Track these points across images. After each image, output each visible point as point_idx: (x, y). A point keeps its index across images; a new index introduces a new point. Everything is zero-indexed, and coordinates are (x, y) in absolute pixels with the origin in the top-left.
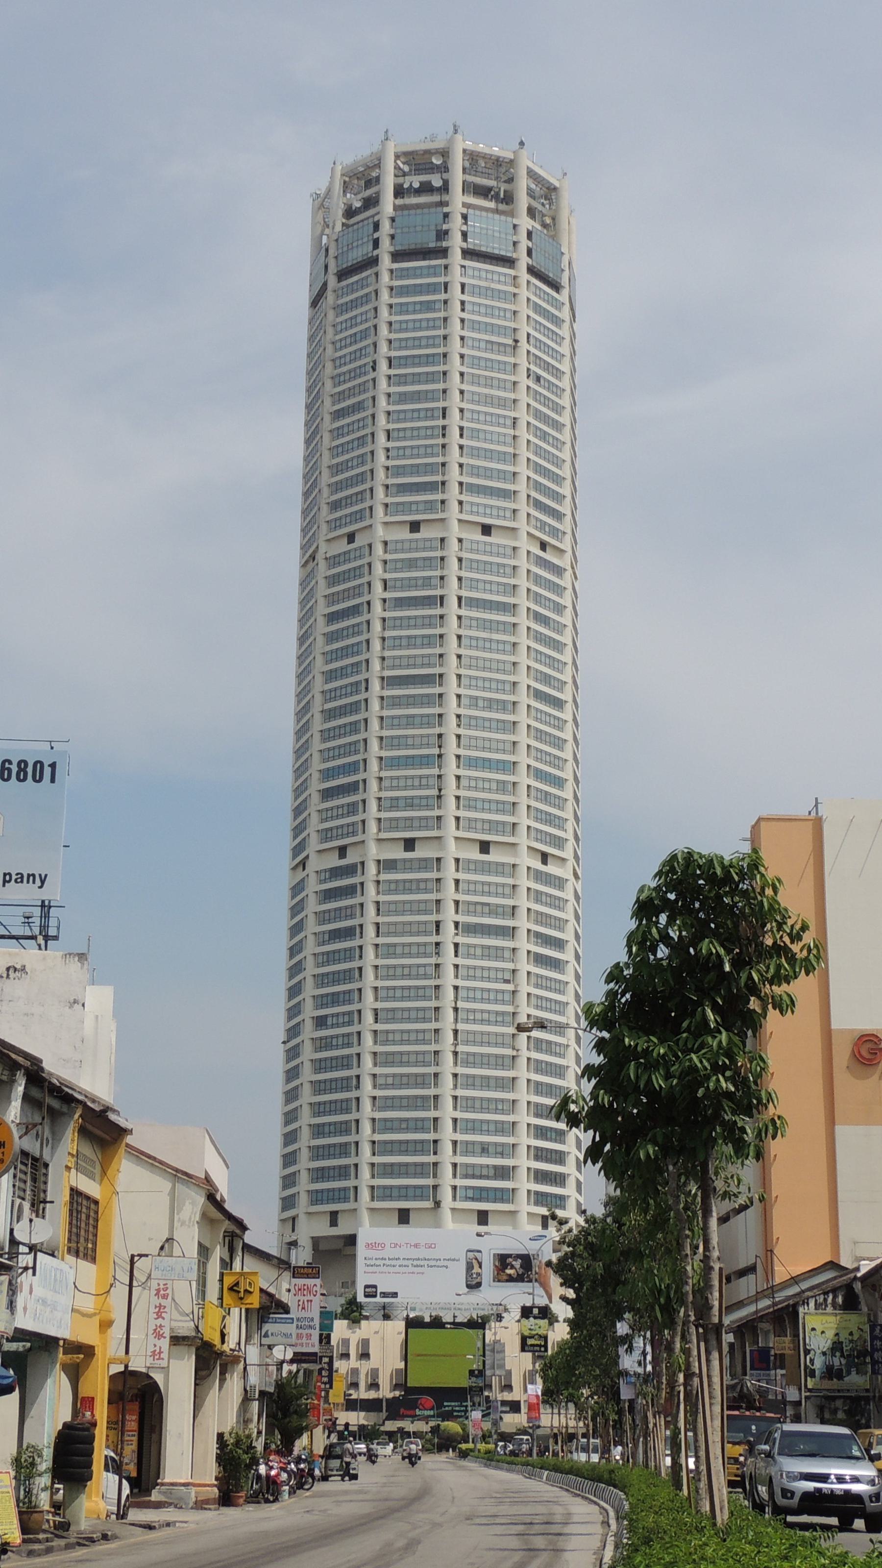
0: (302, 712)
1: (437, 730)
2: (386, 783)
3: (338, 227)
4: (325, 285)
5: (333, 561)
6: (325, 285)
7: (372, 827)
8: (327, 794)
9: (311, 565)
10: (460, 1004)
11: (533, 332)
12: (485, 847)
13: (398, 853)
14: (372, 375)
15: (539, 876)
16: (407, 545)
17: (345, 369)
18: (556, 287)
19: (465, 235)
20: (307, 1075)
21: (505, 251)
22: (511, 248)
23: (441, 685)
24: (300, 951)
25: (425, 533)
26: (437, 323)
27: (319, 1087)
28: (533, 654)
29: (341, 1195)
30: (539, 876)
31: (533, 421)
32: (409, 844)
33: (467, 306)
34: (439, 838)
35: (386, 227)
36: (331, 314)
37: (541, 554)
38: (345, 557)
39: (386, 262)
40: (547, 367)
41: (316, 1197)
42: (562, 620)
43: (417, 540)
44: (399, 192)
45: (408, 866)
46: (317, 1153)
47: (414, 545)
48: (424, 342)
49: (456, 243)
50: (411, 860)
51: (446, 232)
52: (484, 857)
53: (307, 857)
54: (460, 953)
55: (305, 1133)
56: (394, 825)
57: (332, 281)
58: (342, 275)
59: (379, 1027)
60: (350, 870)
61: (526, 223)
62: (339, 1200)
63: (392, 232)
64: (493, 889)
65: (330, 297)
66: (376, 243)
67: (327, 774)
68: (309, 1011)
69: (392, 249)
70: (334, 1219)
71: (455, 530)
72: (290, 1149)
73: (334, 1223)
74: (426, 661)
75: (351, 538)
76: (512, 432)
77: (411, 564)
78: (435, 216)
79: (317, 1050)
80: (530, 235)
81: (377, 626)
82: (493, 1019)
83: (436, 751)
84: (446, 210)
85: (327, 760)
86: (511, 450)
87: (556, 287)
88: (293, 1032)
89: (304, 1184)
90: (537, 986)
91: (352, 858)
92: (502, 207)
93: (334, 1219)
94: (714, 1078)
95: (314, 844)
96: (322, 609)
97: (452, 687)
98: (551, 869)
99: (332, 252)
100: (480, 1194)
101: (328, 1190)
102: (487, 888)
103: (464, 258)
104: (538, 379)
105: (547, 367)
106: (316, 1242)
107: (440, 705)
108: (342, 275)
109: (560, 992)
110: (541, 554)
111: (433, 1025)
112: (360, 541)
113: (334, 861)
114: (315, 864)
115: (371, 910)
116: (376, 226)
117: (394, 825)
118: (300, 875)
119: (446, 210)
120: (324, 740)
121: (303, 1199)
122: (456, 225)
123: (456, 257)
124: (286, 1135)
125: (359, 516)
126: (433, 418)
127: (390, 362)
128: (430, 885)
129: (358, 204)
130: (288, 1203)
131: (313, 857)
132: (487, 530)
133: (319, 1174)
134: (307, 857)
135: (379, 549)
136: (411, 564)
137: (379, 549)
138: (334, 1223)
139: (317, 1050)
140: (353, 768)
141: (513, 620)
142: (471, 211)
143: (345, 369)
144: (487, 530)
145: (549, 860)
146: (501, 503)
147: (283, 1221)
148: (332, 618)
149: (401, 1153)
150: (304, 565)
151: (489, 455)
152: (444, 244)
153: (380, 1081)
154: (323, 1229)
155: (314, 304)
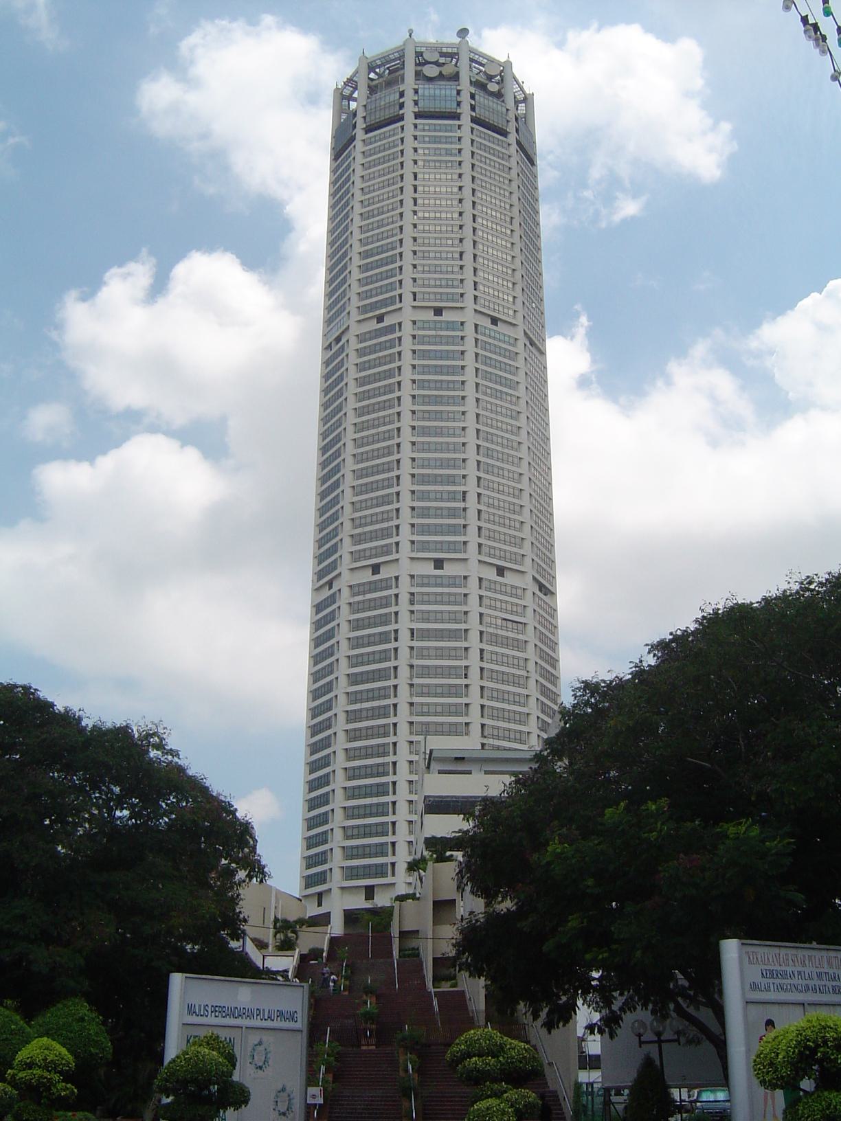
12: (501, 571)
23: (466, 639)
26: (455, 283)
33: (485, 656)
41: (350, 873)
43: (441, 577)
47: (439, 598)
48: (445, 385)
52: (499, 579)
53: (340, 574)
54: (484, 639)
56: (425, 547)
58: (368, 130)
59: (415, 644)
62: (376, 875)
69: (410, 859)
70: (370, 892)
74: (452, 599)
79: (349, 759)
85: (356, 628)
101: (365, 786)
106: (351, 917)
116: (402, 95)
117: (425, 547)
120: (348, 721)
125: (386, 550)
126: (455, 500)
127: (412, 634)
128: (458, 463)
132: (495, 321)
139: (349, 759)
144: (495, 321)
149: (436, 373)
154: (358, 902)
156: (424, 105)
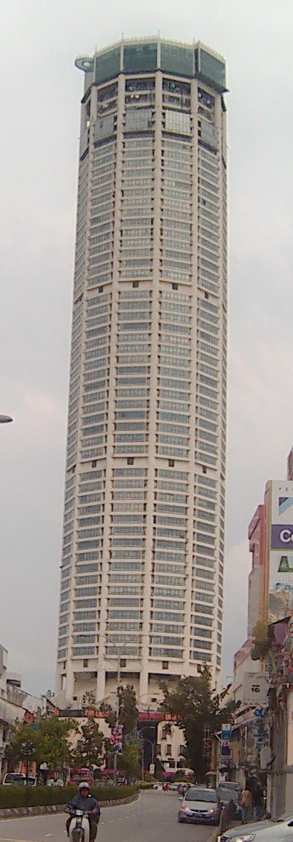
0: (64, 596)
1: (146, 398)
2: (121, 338)
3: (95, 118)
4: (87, 150)
5: (91, 302)
6: (87, 150)
9: (79, 303)
10: (155, 573)
11: (201, 177)
13: (124, 465)
14: (107, 377)
15: (201, 479)
16: (131, 295)
17: (92, 360)
18: (215, 151)
19: (164, 123)
20: (73, 584)
21: (186, 131)
22: (189, 130)
24: (71, 517)
25: (142, 287)
28: (199, 410)
29: (90, 651)
30: (201, 479)
31: (201, 167)
32: (130, 460)
34: (147, 457)
35: (121, 119)
36: (91, 166)
37: (205, 299)
39: (120, 138)
42: (217, 358)
44: (128, 99)
45: (130, 472)
46: (79, 604)
49: (158, 128)
50: (131, 469)
51: (154, 122)
58: (96, 145)
60: (97, 474)
61: (196, 117)
63: (124, 112)
64: (172, 605)
65: (91, 156)
66: (115, 127)
68: (75, 539)
71: (156, 286)
72: (63, 625)
73: (85, 666)
75: (101, 289)
76: (189, 153)
78: (147, 114)
80: (199, 123)
81: (114, 338)
82: (177, 441)
83: (146, 409)
84: (153, 110)
86: (189, 252)
87: (215, 151)
89: (70, 643)
90: (200, 493)
91: (100, 466)
92: (185, 108)
95: (79, 459)
97: (154, 373)
98: (210, 300)
99: (92, 132)
100: (168, 652)
102: (172, 486)
103: (163, 136)
104: (204, 202)
107: (149, 372)
108: (96, 145)
109: (215, 354)
110: (205, 299)
111: (145, 444)
112: (106, 291)
113: (89, 468)
114: (80, 469)
116: (116, 118)
117: (122, 449)
118: (72, 475)
119: (153, 110)
120: (84, 401)
121: (70, 652)
122: (158, 118)
123: (159, 136)
124: (62, 606)
129: (106, 106)
130: (61, 653)
131: (78, 466)
132: (175, 286)
133: (79, 638)
134: (75, 466)
135: (116, 296)
137: (116, 296)
138: (85, 666)
140: (100, 417)
141: (187, 425)
142: (167, 111)
143: (92, 360)
144: (175, 286)
145: (208, 471)
146: (184, 271)
147: (59, 663)
148: (87, 388)
150: (76, 303)
152: (153, 129)
153: (112, 590)
155: (82, 159)
156: (132, 126)
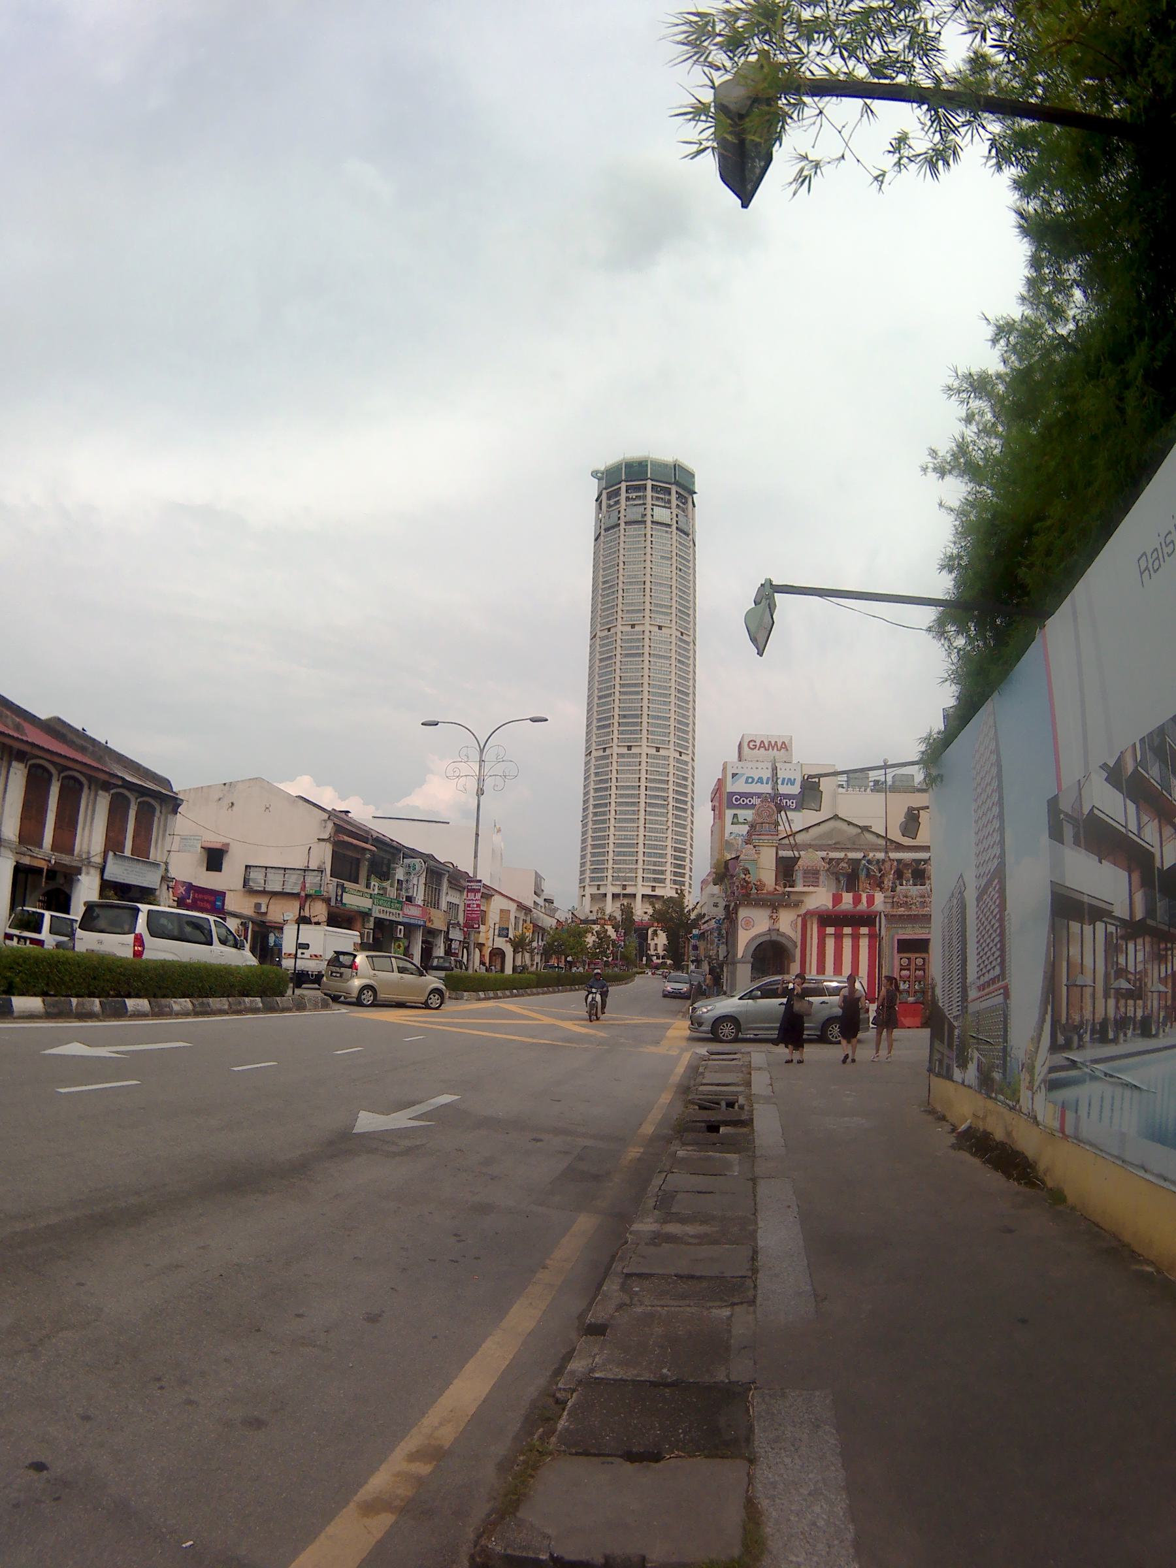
5: (602, 639)
7: (615, 740)
8: (599, 728)
13: (625, 751)
15: (678, 761)
18: (688, 535)
25: (637, 628)
27: (596, 790)
32: (629, 748)
38: (607, 637)
39: (623, 525)
40: (684, 565)
44: (628, 499)
45: (629, 756)
49: (649, 519)
55: (589, 855)
56: (624, 740)
57: (603, 532)
58: (606, 530)
60: (606, 757)
61: (675, 511)
65: (602, 538)
67: (599, 720)
70: (599, 887)
71: (647, 628)
75: (609, 630)
77: (631, 641)
78: (641, 509)
81: (618, 663)
88: (585, 817)
93: (599, 887)
94: (728, 64)
95: (594, 747)
96: (598, 656)
97: (646, 688)
98: (685, 637)
100: (655, 880)
102: (658, 765)
105: (684, 565)
108: (606, 530)
112: (613, 631)
113: (601, 753)
114: (594, 754)
115: (614, 772)
117: (624, 740)
121: (588, 880)
122: (649, 512)
123: (649, 524)
130: (582, 881)
132: (660, 628)
136: (631, 641)
137: (619, 634)
144: (660, 628)
151: (661, 606)
154: (595, 891)
